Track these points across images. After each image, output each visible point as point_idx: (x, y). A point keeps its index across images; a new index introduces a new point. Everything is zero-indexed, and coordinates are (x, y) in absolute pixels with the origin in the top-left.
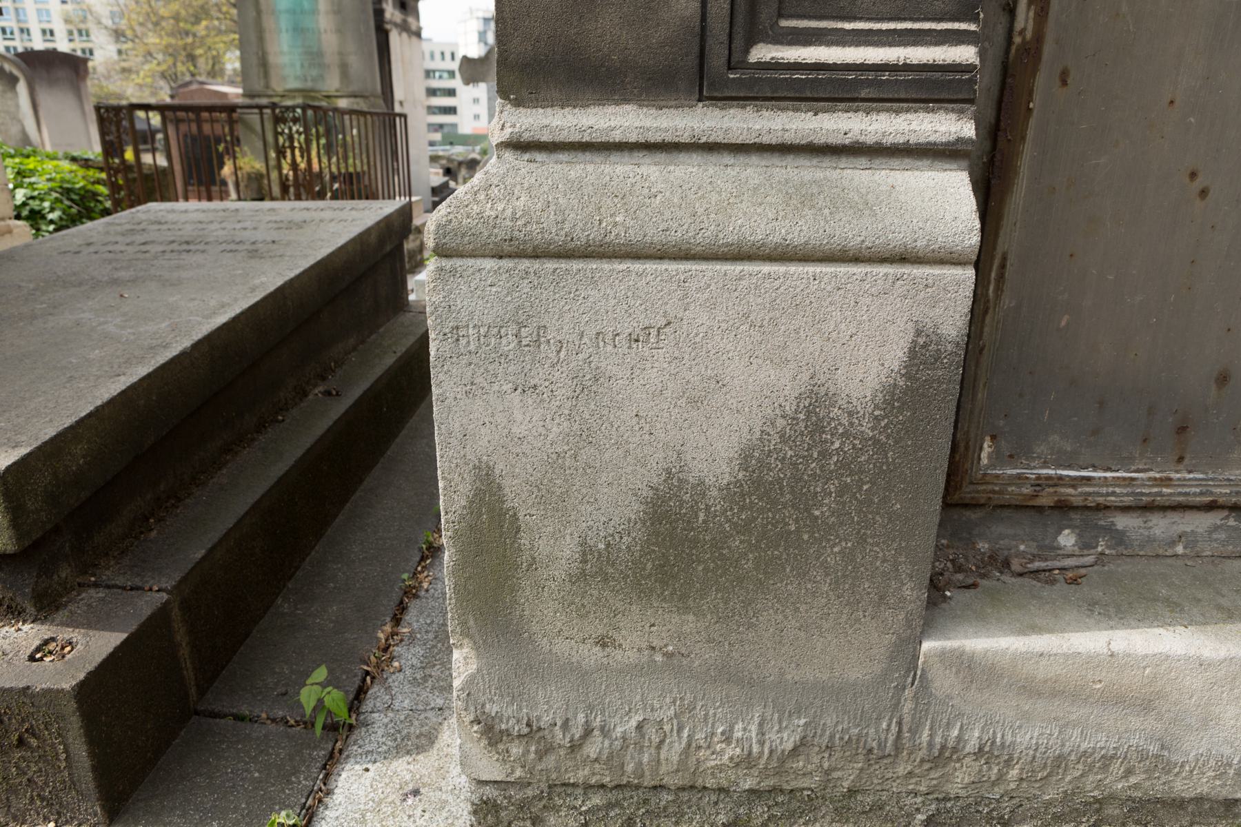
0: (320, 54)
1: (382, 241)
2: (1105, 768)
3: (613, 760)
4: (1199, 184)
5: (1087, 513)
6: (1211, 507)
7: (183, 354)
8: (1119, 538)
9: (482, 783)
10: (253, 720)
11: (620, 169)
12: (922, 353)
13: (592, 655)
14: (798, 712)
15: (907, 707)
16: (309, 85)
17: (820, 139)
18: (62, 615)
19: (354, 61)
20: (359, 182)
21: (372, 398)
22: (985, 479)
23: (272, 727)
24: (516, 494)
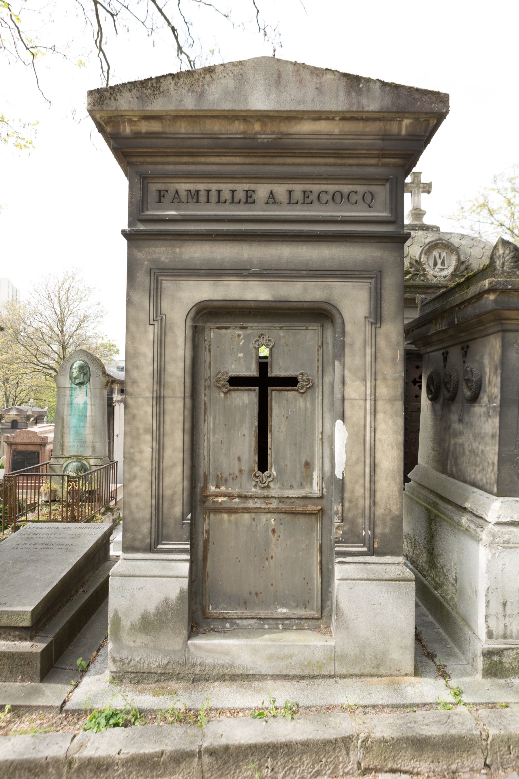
0: (85, 442)
1: (103, 540)
2: (223, 667)
3: (135, 666)
4: (238, 560)
5: (231, 620)
6: (253, 618)
7: (57, 584)
8: (238, 625)
9: (112, 672)
10: (65, 669)
11: (139, 563)
12: (182, 591)
13: (132, 644)
14: (168, 656)
15: (187, 654)
16: (79, 454)
17: (167, 559)
18: (34, 641)
19: (98, 446)
20: (95, 494)
21: (96, 592)
22: (210, 613)
23: (69, 670)
24: (121, 615)
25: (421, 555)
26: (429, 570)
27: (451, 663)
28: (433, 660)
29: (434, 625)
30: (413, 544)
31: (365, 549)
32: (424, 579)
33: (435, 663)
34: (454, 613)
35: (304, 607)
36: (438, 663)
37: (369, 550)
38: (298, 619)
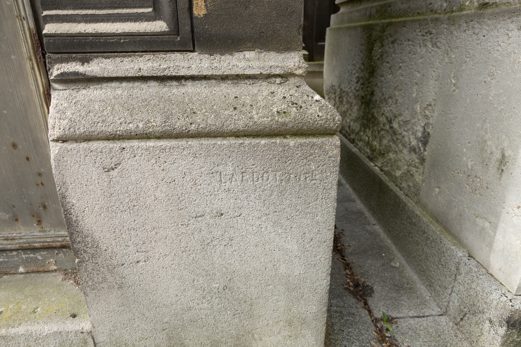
25: (349, 112)
26: (360, 130)
27: (405, 312)
28: (366, 303)
29: (366, 218)
30: (337, 99)
31: (159, 26)
32: (351, 146)
33: (370, 312)
34: (411, 204)
35: (35, 220)
36: (378, 314)
37: (175, 28)
38: (25, 249)
